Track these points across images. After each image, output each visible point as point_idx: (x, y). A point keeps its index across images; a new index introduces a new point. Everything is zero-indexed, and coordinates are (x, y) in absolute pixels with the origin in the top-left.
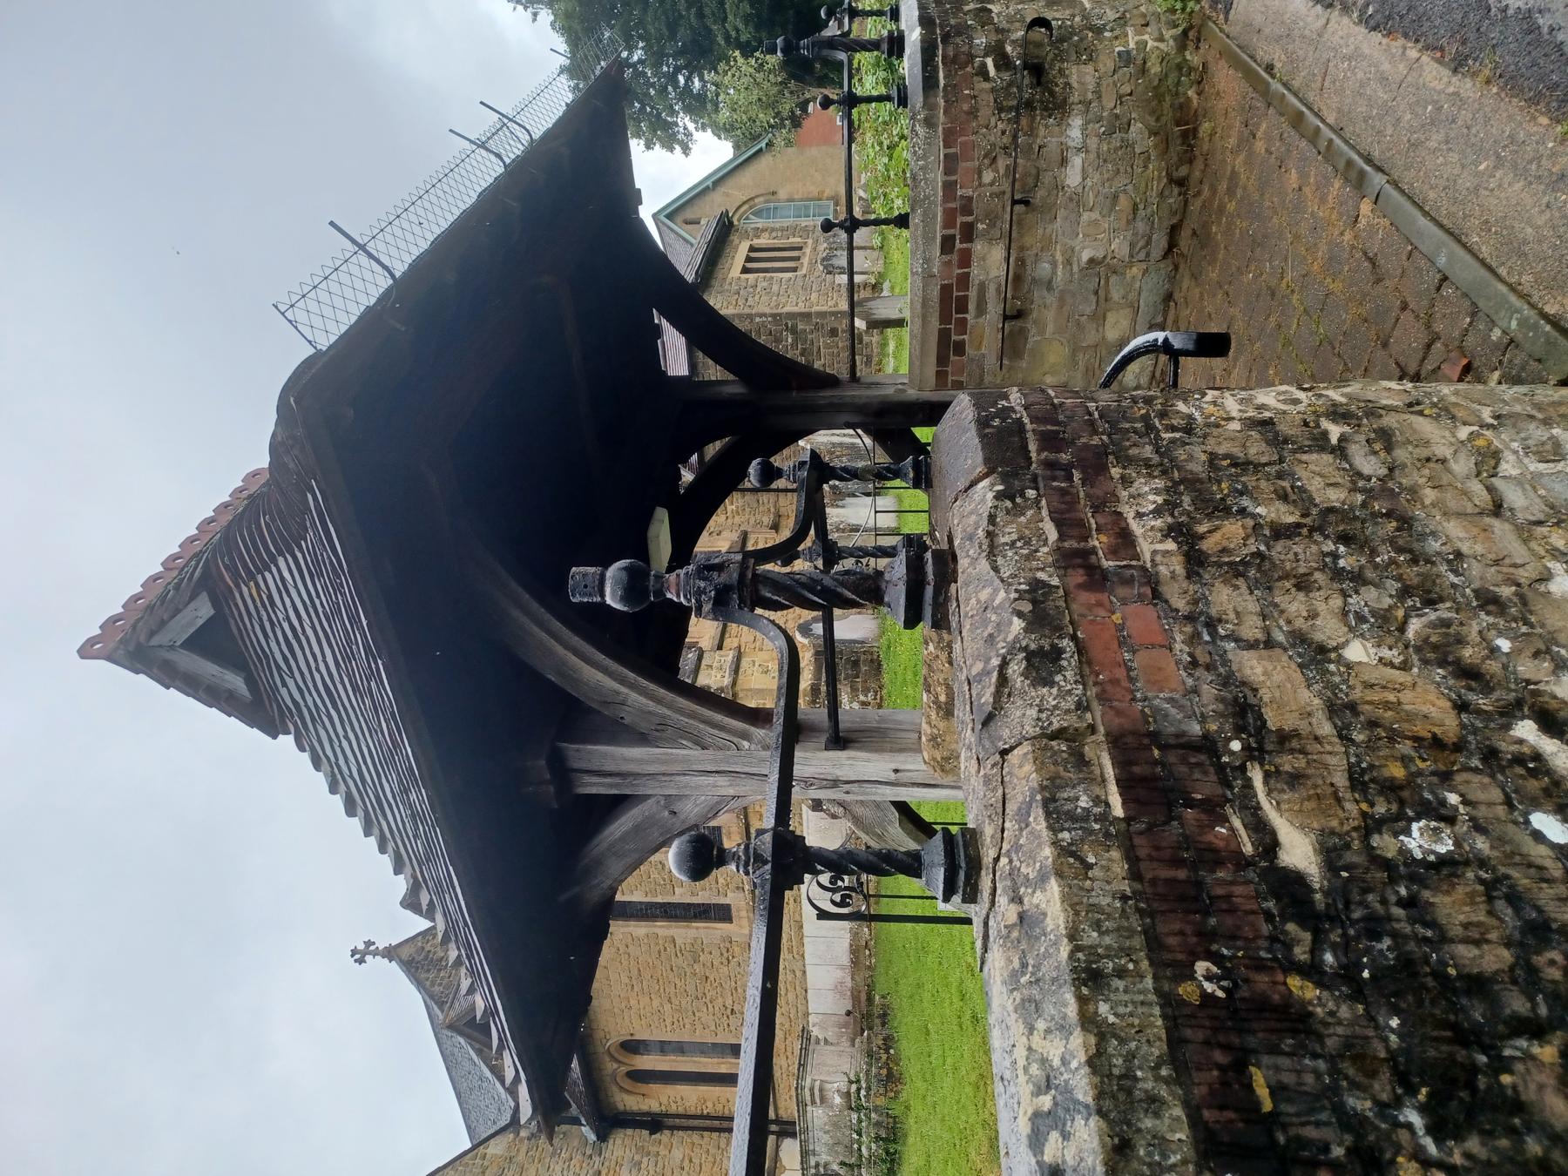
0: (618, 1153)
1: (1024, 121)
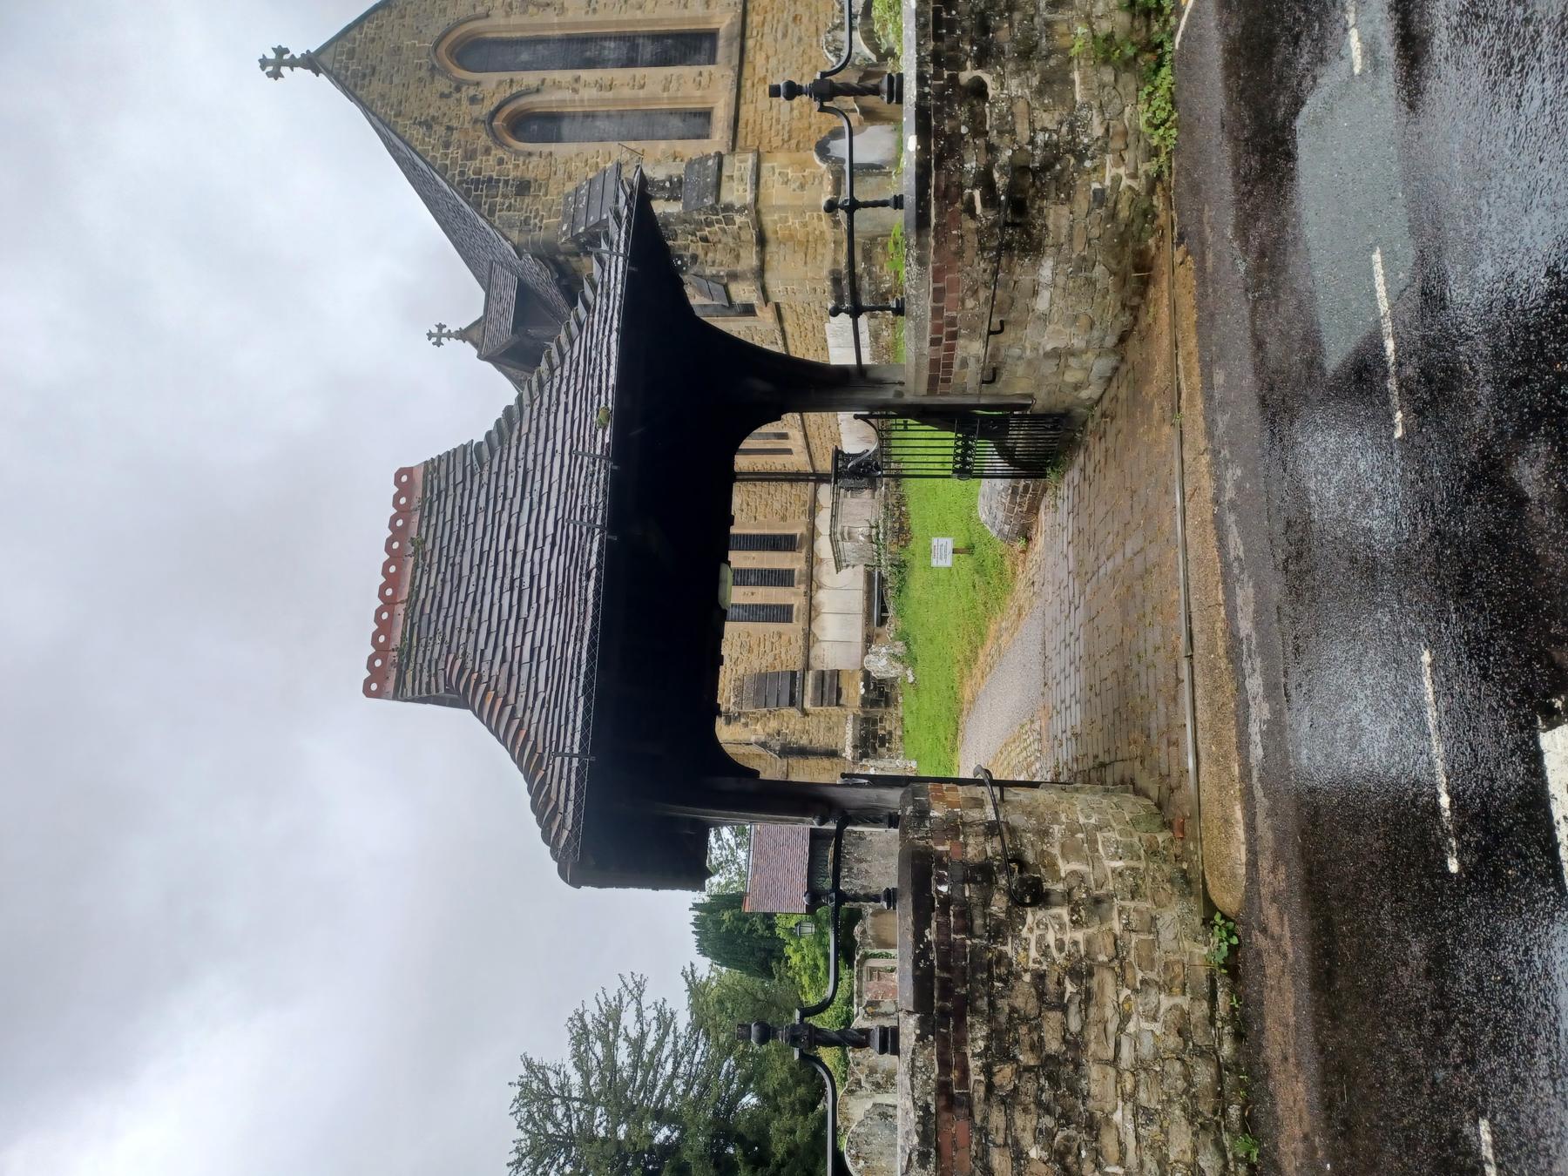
1: (1004, 261)
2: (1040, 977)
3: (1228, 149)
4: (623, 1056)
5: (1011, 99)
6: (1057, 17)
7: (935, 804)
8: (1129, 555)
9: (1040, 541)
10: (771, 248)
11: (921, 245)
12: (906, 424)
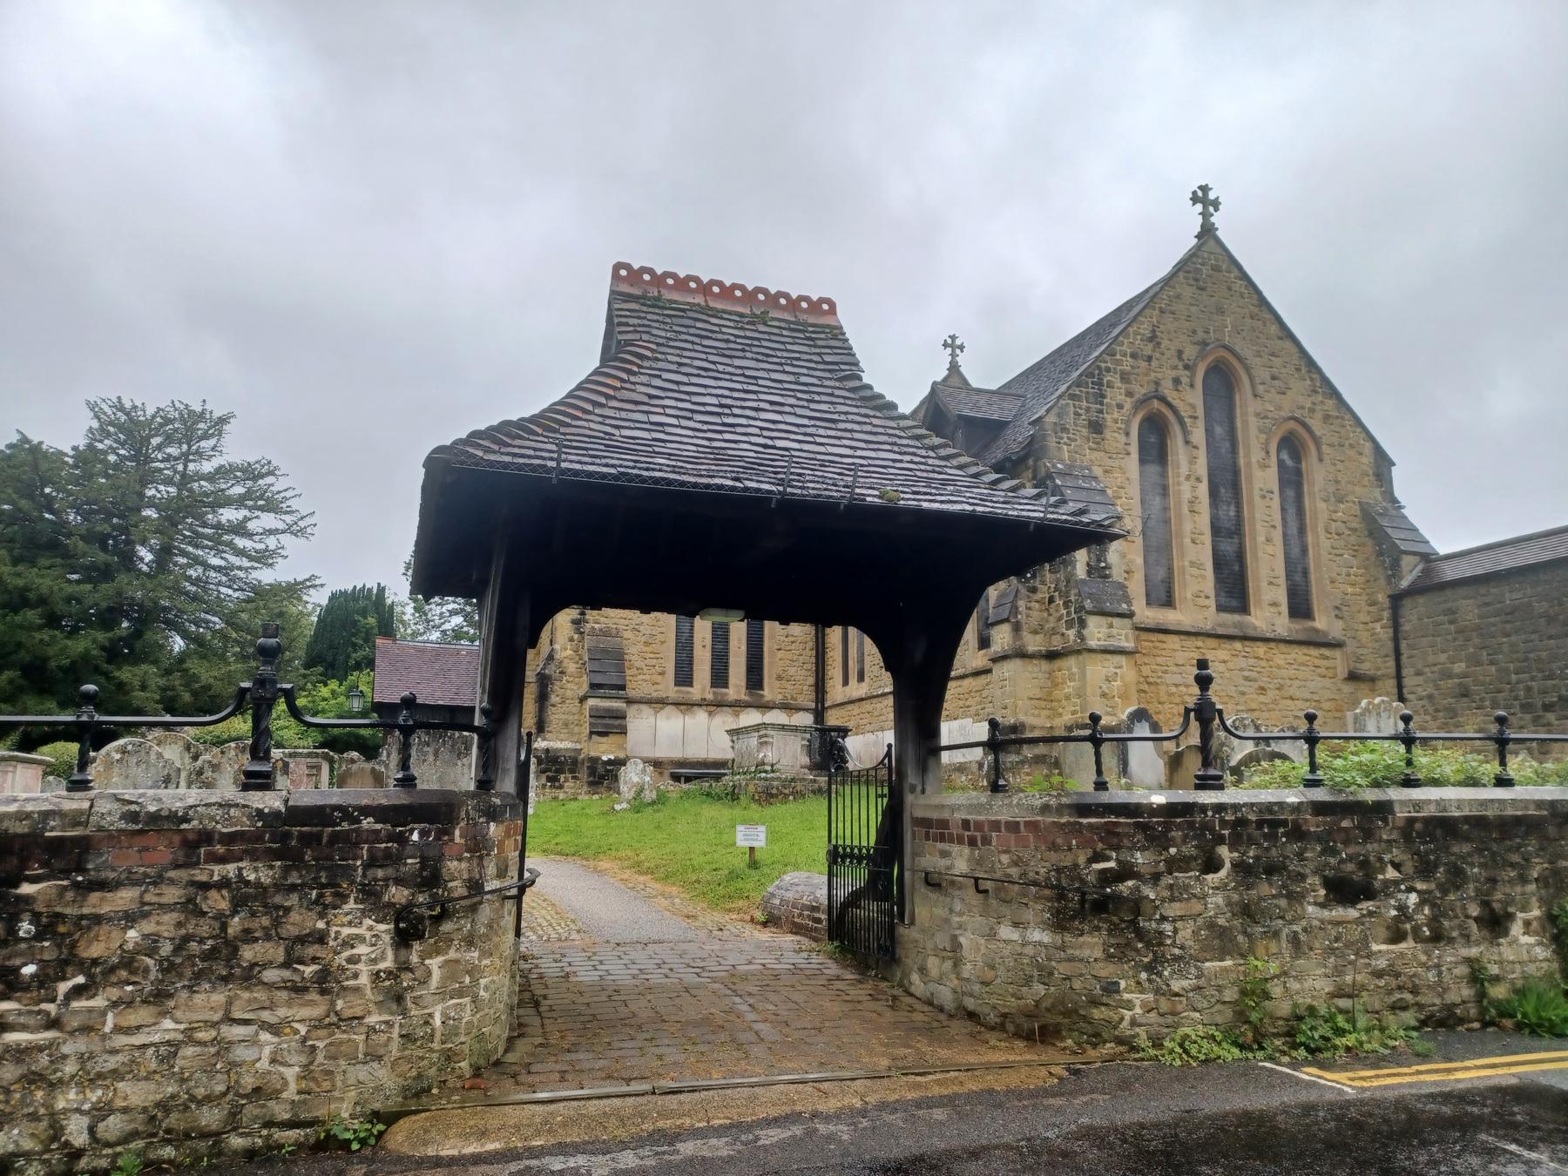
1: (1047, 892)
2: (321, 938)
3: (1166, 1117)
4: (229, 515)
5: (1204, 896)
6: (1284, 944)
7: (502, 828)
8: (757, 1026)
9: (765, 936)
10: (1045, 665)
11: (1060, 809)
12: (883, 796)
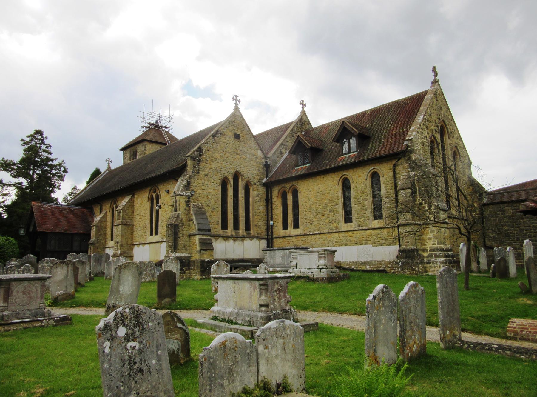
0: (260, 190)
